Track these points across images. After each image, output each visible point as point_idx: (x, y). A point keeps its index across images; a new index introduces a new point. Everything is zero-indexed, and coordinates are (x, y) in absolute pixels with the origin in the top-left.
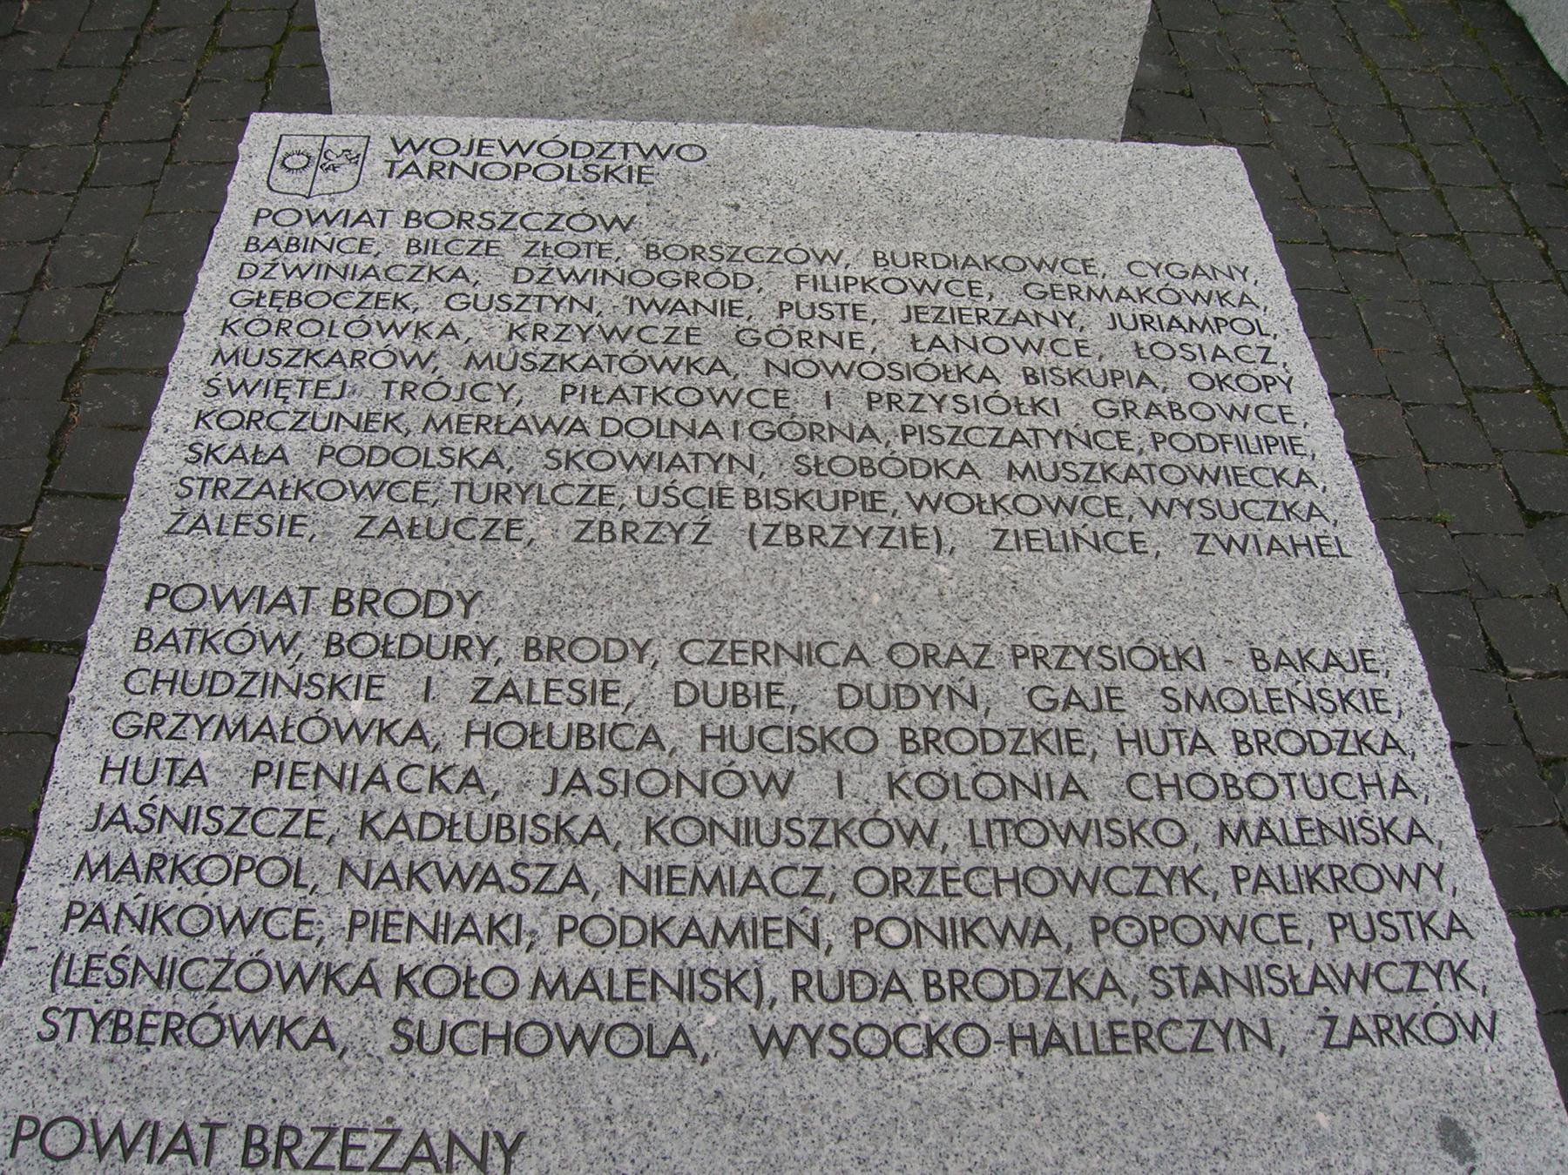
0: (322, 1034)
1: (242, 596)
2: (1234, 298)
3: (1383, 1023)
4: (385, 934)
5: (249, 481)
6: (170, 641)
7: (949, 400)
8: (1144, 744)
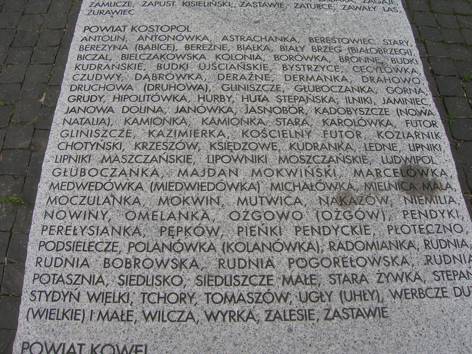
4: (309, 317)
7: (294, 66)
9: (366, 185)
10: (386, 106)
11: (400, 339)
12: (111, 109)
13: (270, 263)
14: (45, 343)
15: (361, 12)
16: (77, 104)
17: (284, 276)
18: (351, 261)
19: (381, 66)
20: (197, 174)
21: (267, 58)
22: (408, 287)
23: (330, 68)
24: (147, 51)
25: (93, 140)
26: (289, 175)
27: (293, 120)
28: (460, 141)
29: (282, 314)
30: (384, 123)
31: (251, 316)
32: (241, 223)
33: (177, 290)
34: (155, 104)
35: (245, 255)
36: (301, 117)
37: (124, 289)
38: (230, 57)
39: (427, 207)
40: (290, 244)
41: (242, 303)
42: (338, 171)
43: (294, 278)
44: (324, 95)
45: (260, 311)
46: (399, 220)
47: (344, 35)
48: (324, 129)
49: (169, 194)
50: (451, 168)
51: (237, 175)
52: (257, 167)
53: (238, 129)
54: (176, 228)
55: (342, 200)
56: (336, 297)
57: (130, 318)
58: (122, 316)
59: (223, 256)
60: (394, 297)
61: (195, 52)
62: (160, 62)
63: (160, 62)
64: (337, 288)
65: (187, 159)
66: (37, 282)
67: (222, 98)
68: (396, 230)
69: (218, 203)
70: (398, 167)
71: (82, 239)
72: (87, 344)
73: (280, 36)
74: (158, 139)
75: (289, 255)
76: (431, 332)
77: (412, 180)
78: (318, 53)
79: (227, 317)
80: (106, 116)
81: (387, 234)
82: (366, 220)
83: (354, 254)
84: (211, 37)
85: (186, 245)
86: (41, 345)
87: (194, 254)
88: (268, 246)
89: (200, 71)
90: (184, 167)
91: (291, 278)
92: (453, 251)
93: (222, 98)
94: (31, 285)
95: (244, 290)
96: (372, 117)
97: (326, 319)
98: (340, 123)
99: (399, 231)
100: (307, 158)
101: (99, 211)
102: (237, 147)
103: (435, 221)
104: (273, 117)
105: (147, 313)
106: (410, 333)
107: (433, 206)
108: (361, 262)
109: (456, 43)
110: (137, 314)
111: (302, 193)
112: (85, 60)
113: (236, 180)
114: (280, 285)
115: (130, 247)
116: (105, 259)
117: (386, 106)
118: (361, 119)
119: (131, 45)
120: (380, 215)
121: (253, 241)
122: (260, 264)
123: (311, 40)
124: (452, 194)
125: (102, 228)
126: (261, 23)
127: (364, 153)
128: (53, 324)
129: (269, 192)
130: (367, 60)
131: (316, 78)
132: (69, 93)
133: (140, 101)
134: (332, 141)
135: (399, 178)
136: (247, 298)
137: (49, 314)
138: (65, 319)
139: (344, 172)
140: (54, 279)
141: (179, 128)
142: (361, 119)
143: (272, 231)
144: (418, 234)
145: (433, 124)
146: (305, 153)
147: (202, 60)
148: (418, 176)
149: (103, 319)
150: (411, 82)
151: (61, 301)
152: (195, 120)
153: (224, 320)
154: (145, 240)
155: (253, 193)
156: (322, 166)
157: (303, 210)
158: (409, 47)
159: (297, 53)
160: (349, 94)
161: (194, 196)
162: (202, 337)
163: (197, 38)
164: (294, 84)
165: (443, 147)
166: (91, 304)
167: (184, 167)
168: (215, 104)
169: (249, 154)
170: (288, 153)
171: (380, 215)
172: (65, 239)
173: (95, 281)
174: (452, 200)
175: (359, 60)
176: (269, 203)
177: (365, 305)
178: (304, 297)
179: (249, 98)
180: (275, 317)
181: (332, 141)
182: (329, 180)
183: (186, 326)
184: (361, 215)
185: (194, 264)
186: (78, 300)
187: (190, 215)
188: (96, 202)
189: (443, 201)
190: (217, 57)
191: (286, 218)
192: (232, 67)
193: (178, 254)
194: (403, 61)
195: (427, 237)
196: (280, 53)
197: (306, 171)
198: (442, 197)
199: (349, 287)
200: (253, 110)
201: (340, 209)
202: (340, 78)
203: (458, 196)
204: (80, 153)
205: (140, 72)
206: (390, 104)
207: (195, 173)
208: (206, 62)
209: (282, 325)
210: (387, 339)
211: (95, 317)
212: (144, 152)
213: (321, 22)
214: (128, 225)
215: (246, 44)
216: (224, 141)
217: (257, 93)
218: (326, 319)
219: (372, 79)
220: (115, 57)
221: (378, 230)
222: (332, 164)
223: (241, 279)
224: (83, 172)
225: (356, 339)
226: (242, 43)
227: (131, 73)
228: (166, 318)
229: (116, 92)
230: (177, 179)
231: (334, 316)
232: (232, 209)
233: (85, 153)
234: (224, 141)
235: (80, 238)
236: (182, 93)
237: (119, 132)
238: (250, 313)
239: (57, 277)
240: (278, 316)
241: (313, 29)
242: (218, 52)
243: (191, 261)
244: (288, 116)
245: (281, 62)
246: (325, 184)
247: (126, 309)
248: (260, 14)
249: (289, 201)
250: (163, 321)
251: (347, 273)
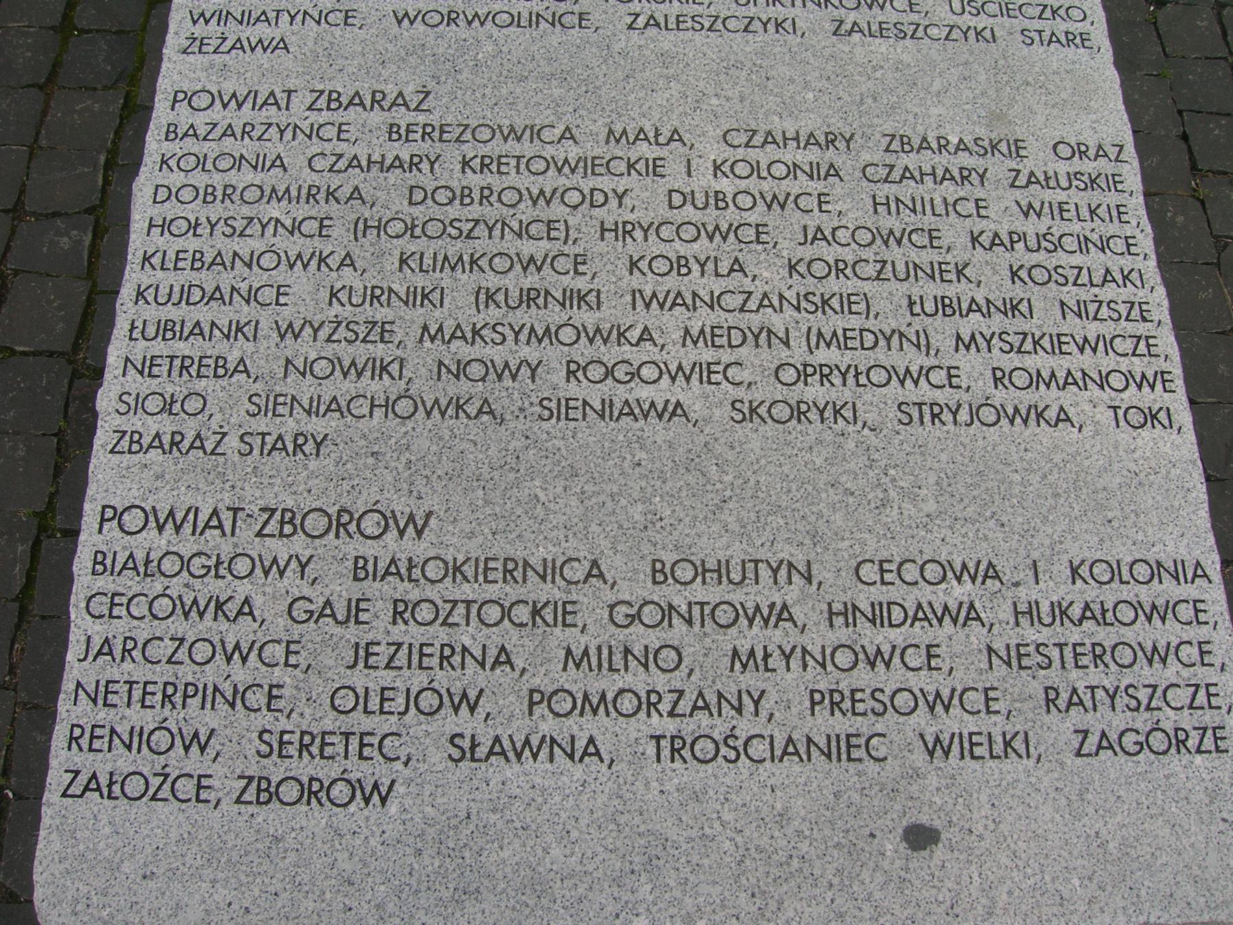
1: (208, 16)
3: (965, 173)
5: (340, 156)
6: (278, 163)
58: (110, 786)
86: (252, 560)
133: (519, 26)
173: (185, 334)
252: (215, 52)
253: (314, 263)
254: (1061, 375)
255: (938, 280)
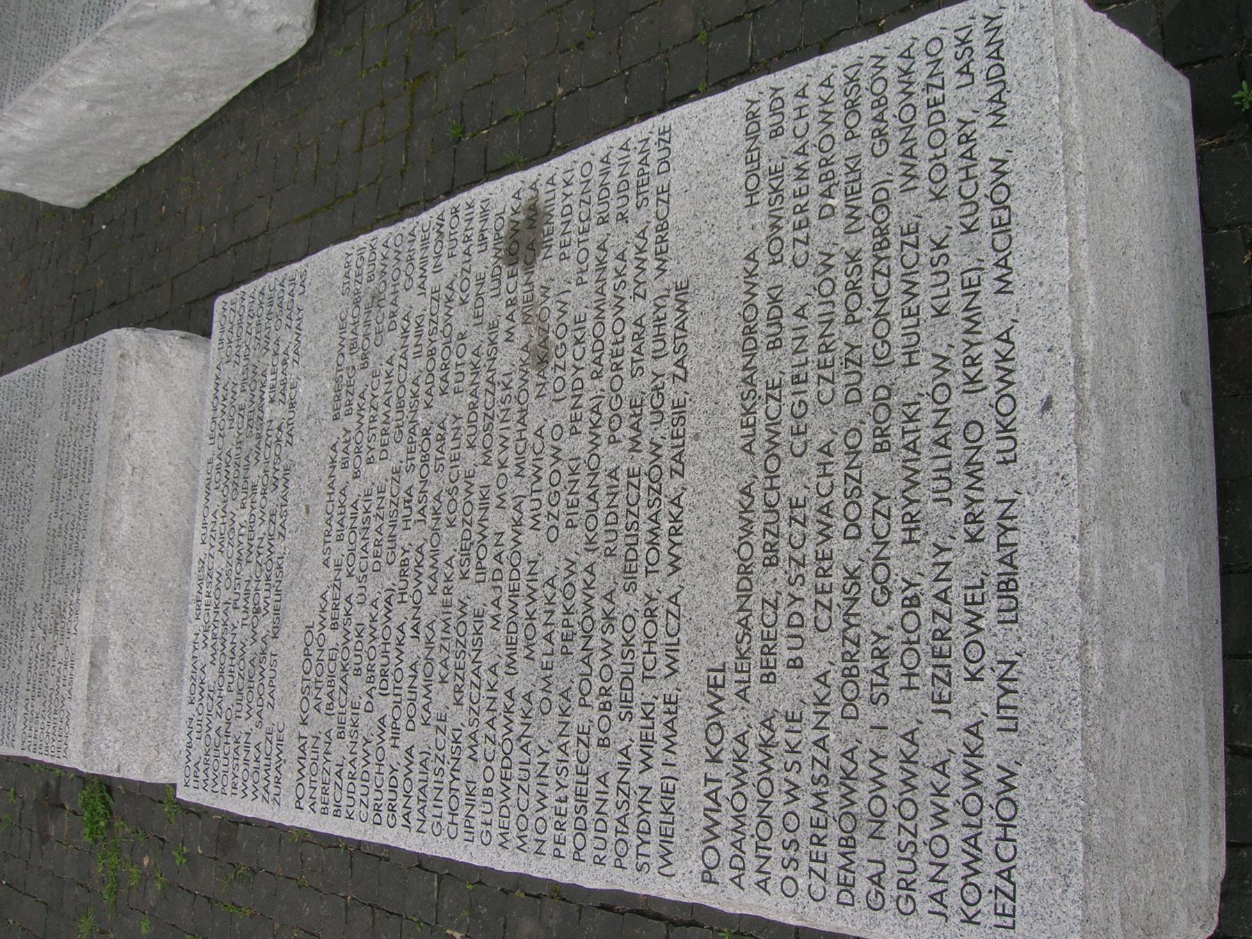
0: (940, 768)
2: (825, 93)
8: (912, 349)
9: (525, 323)
10: (428, 292)
11: (716, 259)
12: (409, 751)
13: (612, 474)
14: (704, 842)
15: (303, 333)
16: (400, 811)
17: (631, 450)
18: (617, 343)
19: (377, 298)
20: (498, 599)
21: (356, 491)
22: (653, 250)
23: (375, 385)
24: (336, 696)
25: (447, 779)
26: (506, 448)
27: (439, 444)
28: (553, 141)
29: (676, 451)
30: (449, 293)
31: (676, 502)
32: (561, 525)
33: (641, 622)
34: (406, 675)
35: (601, 514)
36: (436, 430)
37: (637, 712)
38: (352, 552)
39: (557, 221)
40: (591, 442)
41: (661, 515)
42: (506, 369)
43: (633, 434)
44: (409, 394)
45: (671, 486)
46: (570, 267)
47: (333, 363)
48: (452, 394)
49: (521, 645)
50: (512, 181)
51: (502, 534)
52: (494, 501)
53: (445, 535)
54: (564, 630)
55: (542, 361)
56: (659, 366)
57: (673, 699)
59: (602, 549)
60: (665, 271)
61: (342, 612)
62: (350, 672)
63: (350, 672)
64: (649, 365)
65: (479, 616)
66: (625, 861)
67: (404, 564)
68: (582, 271)
69: (536, 562)
70: (506, 270)
71: (572, 785)
72: (705, 769)
73: (328, 470)
74: (452, 668)
75: (605, 442)
76: (711, 208)
77: (523, 247)
78: (355, 406)
79: (676, 539)
80: (417, 759)
81: (586, 286)
82: (568, 320)
83: (609, 338)
84: (323, 585)
85: (970, 634)
87: (597, 597)
88: (592, 477)
89: (368, 602)
90: (489, 622)
91: (632, 439)
92: (613, 179)
93: (404, 564)
94: (628, 872)
95: (645, 513)
96: (441, 315)
97: (685, 380)
98: (446, 367)
99: (584, 267)
100: (488, 420)
101: (538, 760)
102: (467, 535)
103: (575, 207)
104: (432, 478)
105: (668, 671)
106: (709, 243)
107: (556, 212)
108: (618, 328)
109: (406, 148)
110: (668, 688)
111: (530, 425)
112: (341, 803)
113: (509, 534)
114: (641, 455)
115: (585, 705)
116: (599, 745)
117: (428, 292)
118: (442, 332)
119: (325, 723)
120: (563, 297)
121: (585, 502)
122: (614, 490)
123: (336, 418)
124: (543, 180)
125: (560, 753)
126: (310, 502)
127: (486, 327)
128: (679, 829)
129: (526, 479)
130: (367, 324)
131: (387, 409)
132: (384, 829)
134: (468, 378)
135: (519, 268)
136: (654, 509)
137: (666, 837)
138: (673, 810)
139: (509, 357)
140: (622, 832)
141: (439, 633)
142: (442, 332)
143: (573, 473)
144: (590, 235)
145: (455, 213)
146: (480, 424)
147: (353, 599)
148: (518, 237)
149: (673, 744)
150: (400, 249)
151: (650, 818)
152: (431, 605)
153: (680, 544)
154: (577, 680)
155: (526, 505)
156: (498, 395)
157: (550, 424)
158: (354, 251)
159: (353, 441)
160: (410, 353)
161: (525, 602)
162: (701, 579)
163: (323, 611)
164: (392, 444)
165: (485, 195)
166: (655, 766)
167: (489, 622)
168: (412, 574)
169: (477, 515)
170: (480, 450)
171: (563, 297)
172: (572, 815)
174: (551, 182)
175: (366, 337)
176: (539, 478)
177: (672, 316)
178: (657, 417)
179: (406, 519)
180: (680, 462)
181: (468, 378)
182: (515, 384)
183: (685, 605)
184: (562, 328)
185: (609, 597)
186: (649, 789)
187: (548, 608)
188: (526, 767)
189: (551, 195)
190: (350, 575)
191: (559, 450)
192: (364, 549)
193: (596, 624)
194: (372, 263)
195: (594, 221)
196: (351, 469)
197: (502, 421)
198: (546, 197)
199: (649, 346)
200: (421, 512)
201: (552, 364)
202: (388, 367)
203: (548, 170)
204: (463, 801)
205: (362, 707)
206: (427, 284)
207: (496, 603)
208: (356, 592)
209: (689, 450)
210: (715, 281)
211: (671, 758)
212: (466, 690)
213: (313, 401)
214: (557, 710)
215: (336, 526)
216: (458, 557)
217: (401, 506)
218: (685, 380)
219: (393, 315)
220: (340, 750)
221: (580, 300)
222: (497, 378)
223: (632, 519)
224: (488, 792)
225: (712, 330)
226: (334, 533)
227: (364, 719)
228: (675, 640)
229: (387, 745)
230: (503, 631)
231: (682, 367)
232: (544, 539)
233: (463, 790)
234: (458, 557)
235: (569, 792)
236: (394, 631)
237: (440, 734)
238: (672, 502)
239: (620, 828)
240: (677, 459)
241: (321, 415)
242: (343, 574)
243: (605, 602)
244: (433, 453)
245: (363, 467)
246: (521, 389)
247: (662, 706)
248: (297, 505)
249: (538, 448)
250: (678, 644)
251: (631, 349)
252: (1013, 900)
253: (1006, 365)
254: (1000, 272)
255: (977, 289)
